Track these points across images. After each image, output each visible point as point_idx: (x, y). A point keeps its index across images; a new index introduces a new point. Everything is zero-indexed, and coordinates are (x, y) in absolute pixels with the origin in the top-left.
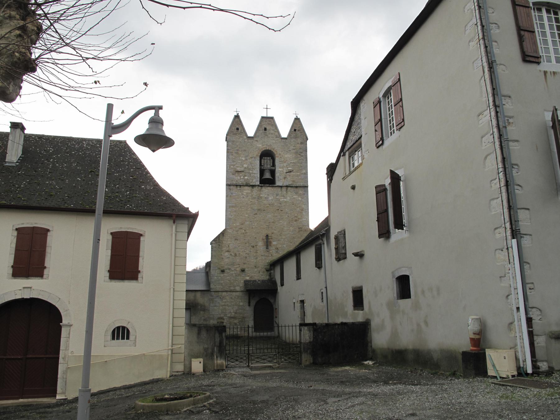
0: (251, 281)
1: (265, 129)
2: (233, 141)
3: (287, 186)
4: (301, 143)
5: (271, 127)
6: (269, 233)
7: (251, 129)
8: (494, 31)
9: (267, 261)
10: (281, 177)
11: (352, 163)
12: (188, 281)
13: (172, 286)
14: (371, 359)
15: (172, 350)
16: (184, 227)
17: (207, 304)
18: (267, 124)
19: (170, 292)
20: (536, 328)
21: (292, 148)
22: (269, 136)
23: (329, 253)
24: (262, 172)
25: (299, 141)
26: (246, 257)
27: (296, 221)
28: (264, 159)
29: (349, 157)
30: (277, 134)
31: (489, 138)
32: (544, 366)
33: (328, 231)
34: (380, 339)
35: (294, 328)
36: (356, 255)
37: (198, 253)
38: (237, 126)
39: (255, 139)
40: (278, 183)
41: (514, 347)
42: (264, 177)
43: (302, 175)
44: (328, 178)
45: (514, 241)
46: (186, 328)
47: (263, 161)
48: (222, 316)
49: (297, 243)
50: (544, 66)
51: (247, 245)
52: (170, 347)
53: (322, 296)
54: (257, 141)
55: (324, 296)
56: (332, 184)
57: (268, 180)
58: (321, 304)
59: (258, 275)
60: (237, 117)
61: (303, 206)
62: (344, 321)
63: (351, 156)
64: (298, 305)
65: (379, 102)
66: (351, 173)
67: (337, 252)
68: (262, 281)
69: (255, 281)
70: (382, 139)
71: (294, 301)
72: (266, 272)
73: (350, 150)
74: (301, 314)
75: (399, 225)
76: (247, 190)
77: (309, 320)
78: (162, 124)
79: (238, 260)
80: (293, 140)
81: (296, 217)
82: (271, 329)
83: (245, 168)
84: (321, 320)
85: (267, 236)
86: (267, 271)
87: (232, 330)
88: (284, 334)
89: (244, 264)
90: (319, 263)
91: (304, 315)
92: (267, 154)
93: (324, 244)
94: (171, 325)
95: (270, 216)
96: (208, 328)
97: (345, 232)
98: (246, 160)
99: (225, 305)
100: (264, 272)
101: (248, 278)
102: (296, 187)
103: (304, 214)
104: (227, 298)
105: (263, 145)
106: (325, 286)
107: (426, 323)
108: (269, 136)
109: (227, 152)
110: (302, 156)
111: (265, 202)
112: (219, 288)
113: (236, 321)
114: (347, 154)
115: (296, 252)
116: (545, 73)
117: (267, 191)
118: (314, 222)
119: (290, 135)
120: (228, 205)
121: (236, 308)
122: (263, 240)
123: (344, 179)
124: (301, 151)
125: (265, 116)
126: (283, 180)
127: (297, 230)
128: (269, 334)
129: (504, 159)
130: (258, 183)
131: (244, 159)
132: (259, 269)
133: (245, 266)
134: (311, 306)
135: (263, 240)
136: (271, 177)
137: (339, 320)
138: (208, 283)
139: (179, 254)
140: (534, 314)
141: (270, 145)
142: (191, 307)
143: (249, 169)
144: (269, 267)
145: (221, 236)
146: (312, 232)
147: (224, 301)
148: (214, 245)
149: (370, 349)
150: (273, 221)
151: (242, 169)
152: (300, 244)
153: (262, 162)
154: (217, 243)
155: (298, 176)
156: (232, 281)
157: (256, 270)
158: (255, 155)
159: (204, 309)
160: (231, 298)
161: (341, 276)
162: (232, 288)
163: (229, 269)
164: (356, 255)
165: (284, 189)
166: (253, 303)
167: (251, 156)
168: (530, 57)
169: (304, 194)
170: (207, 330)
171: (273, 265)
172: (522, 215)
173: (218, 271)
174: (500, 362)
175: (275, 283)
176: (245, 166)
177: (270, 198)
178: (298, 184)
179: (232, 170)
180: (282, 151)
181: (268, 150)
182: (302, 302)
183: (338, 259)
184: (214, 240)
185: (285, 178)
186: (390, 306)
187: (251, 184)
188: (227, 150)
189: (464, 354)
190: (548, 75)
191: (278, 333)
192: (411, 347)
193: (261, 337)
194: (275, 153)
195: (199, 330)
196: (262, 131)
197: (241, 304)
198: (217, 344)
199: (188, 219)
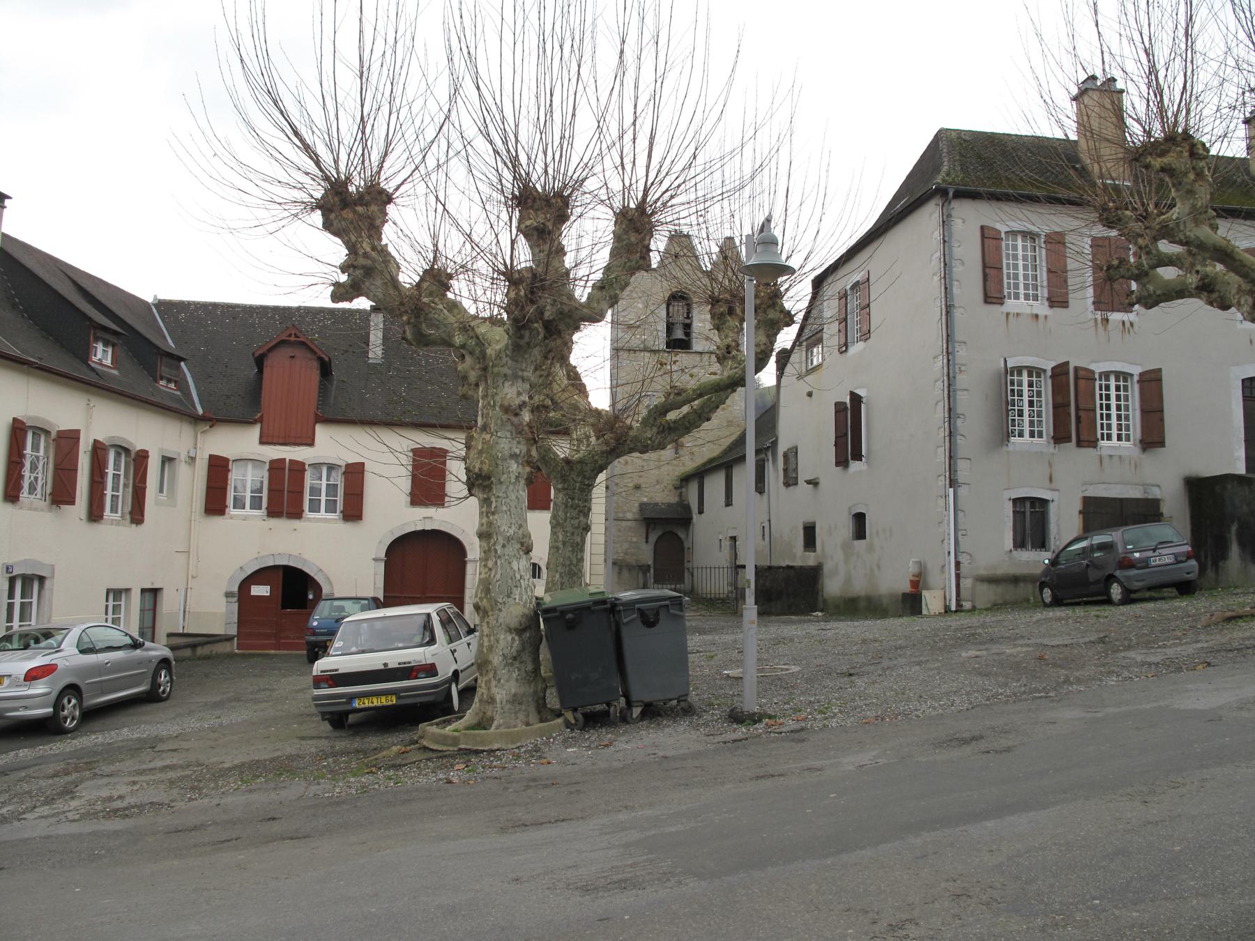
8: (957, 270)
14: (822, 611)
20: (963, 570)
24: (670, 328)
31: (939, 384)
32: (967, 605)
34: (832, 586)
36: (809, 482)
41: (944, 589)
45: (951, 490)
50: (1011, 305)
55: (766, 531)
58: (762, 543)
63: (809, 348)
64: (727, 544)
65: (846, 296)
67: (786, 475)
69: (657, 504)
70: (846, 345)
75: (858, 456)
101: (645, 500)
107: (879, 567)
116: (1008, 314)
121: (626, 545)
129: (950, 409)
130: (663, 346)
133: (641, 481)
137: (784, 564)
140: (964, 560)
149: (820, 598)
161: (789, 508)
162: (621, 515)
164: (809, 482)
166: (653, 538)
168: (992, 296)
171: (685, 480)
172: (962, 465)
174: (932, 601)
175: (687, 508)
182: (734, 539)
183: (787, 484)
186: (846, 547)
189: (904, 594)
190: (1011, 317)
192: (863, 594)
197: (634, 539)
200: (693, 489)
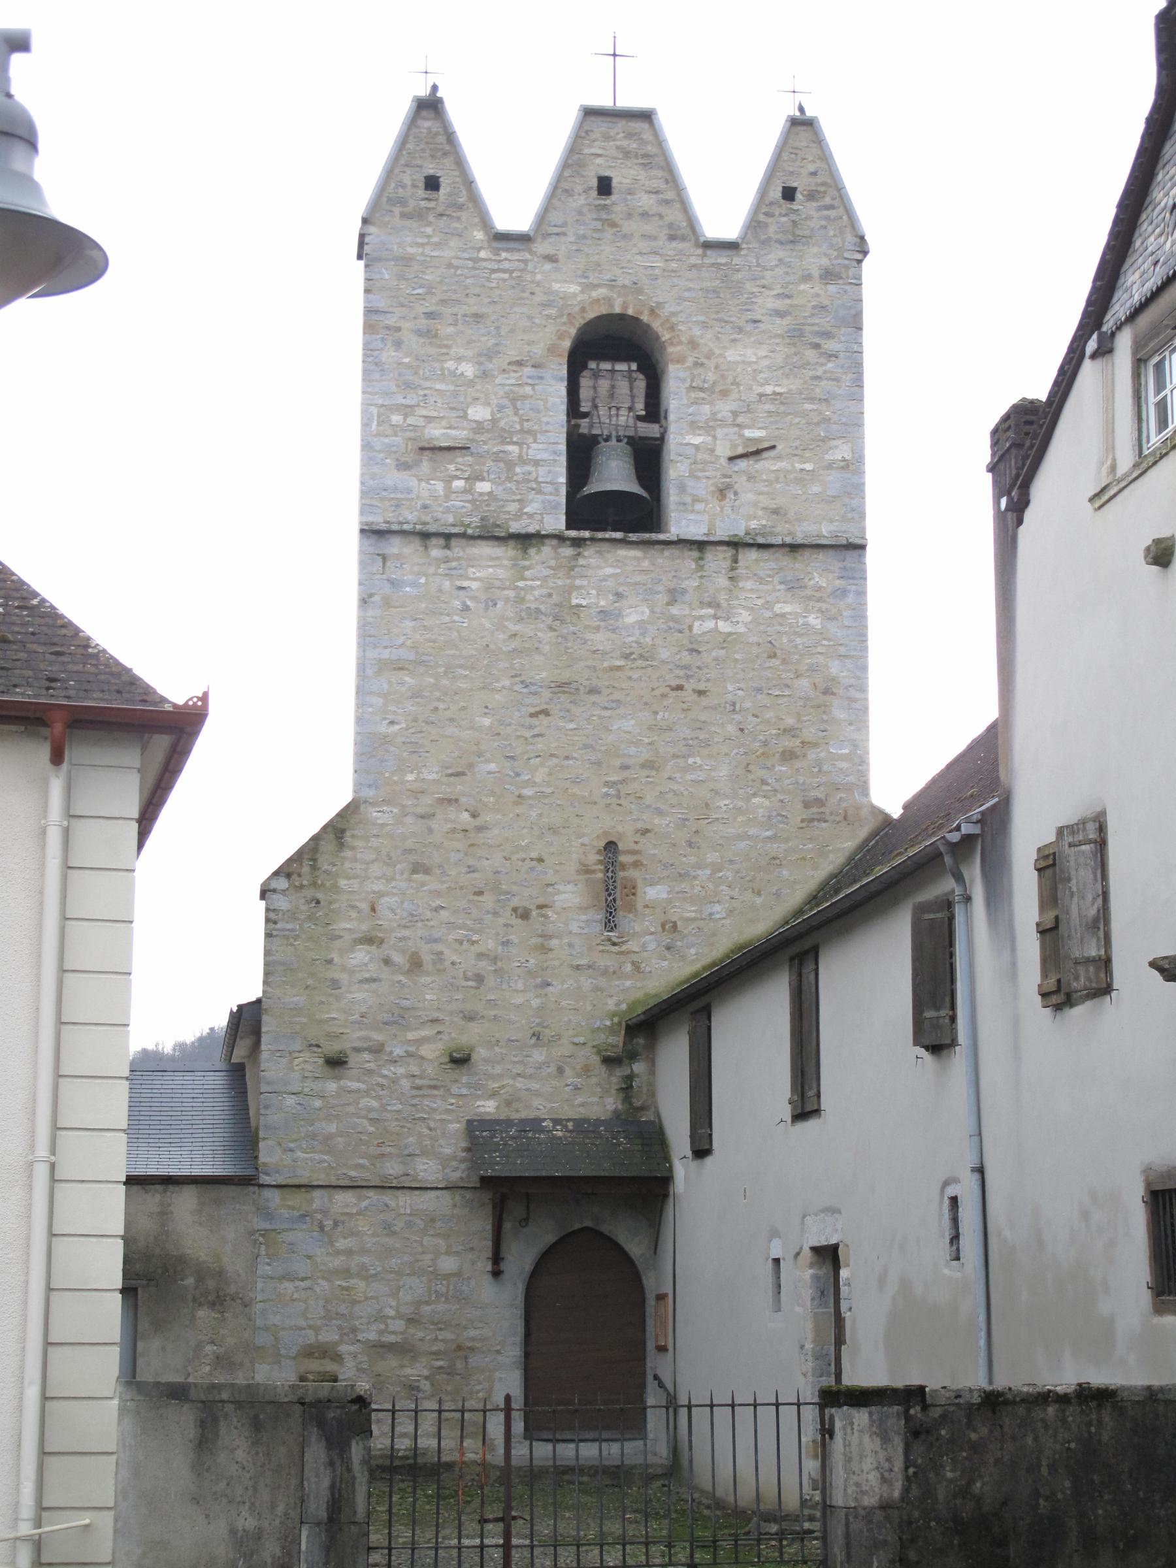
0: (509, 1122)
1: (605, 186)
2: (406, 260)
3: (735, 544)
4: (829, 276)
5: (642, 175)
6: (624, 830)
7: (513, 182)
9: (611, 1004)
10: (702, 488)
11: (1152, 399)
12: (142, 1123)
13: (42, 1151)
15: (38, 1545)
16: (116, 786)
17: (235, 1265)
18: (616, 154)
19: (30, 1188)
21: (772, 303)
22: (629, 226)
23: (999, 960)
24: (581, 453)
25: (815, 258)
26: (480, 979)
27: (789, 756)
28: (596, 375)
29: (1139, 363)
30: (674, 215)
33: (997, 822)
35: (788, 1413)
37: (189, 948)
38: (427, 164)
39: (542, 248)
40: (682, 522)
42: (593, 487)
43: (833, 476)
44: (998, 494)
46: (122, 1410)
47: (585, 382)
48: (329, 1336)
49: (796, 896)
51: (488, 900)
52: (26, 1529)
53: (955, 1221)
54: (551, 259)
55: (967, 1219)
56: (1025, 533)
57: (617, 502)
58: (949, 1271)
59: (553, 1089)
60: (429, 107)
61: (835, 668)
62: (1098, 1378)
64: (801, 1277)
66: (1145, 463)
68: (579, 1123)
69: (535, 1124)
71: (776, 1251)
72: (601, 1070)
73: (1144, 320)
74: (817, 1330)
76: (488, 564)
77: (867, 1368)
78: (31, 144)
79: (429, 994)
80: (775, 254)
81: (789, 732)
82: (630, 1421)
83: (479, 428)
84: (953, 1370)
85: (611, 847)
86: (609, 1061)
87: (428, 1423)
88: (701, 1457)
89: (470, 1018)
90: (936, 1021)
91: (840, 1341)
92: (615, 345)
93: (968, 899)
94: (32, 1393)
95: (629, 724)
96: (259, 1411)
97: (1102, 829)
98: (485, 375)
99: (346, 1273)
100: (587, 1069)
101: (488, 1107)
102: (794, 548)
103: (839, 714)
104: (363, 1225)
105: (587, 287)
106: (971, 1160)
108: (629, 226)
109: (369, 328)
110: (832, 356)
111: (600, 639)
112: (307, 1163)
113: (416, 1371)
114: (1124, 343)
115: (794, 950)
117: (612, 566)
118: (898, 771)
119: (754, 224)
120: (372, 654)
121: (415, 1288)
122: (586, 870)
123: (1101, 498)
124: (825, 322)
125: (606, 102)
126: (714, 505)
127: (797, 814)
128: (613, 1451)
130: (557, 522)
131: (468, 369)
132: (565, 1049)
133: (470, 1035)
134: (882, 1282)
135: (586, 870)
136: (634, 487)
137: (1065, 1376)
138: (245, 1135)
139: (79, 953)
141: (636, 288)
142: (150, 1280)
143: (505, 436)
144: (618, 1040)
145: (327, 847)
146: (887, 832)
147: (341, 1244)
148: (282, 903)
150: (645, 755)
151: (459, 435)
152: (814, 899)
153: (585, 393)
154: (303, 884)
155: (803, 479)
156: (393, 1126)
157: (539, 1056)
158: (538, 350)
159: (219, 1295)
160: (388, 1229)
162: (392, 1168)
163: (377, 1050)
165: (718, 560)
166: (521, 1257)
167: (513, 354)
169: (844, 592)
170: (257, 1425)
171: (645, 1027)
173: (312, 1062)
175: (653, 1139)
176: (479, 413)
177: (631, 618)
178: (802, 532)
179: (403, 444)
180: (705, 326)
181: (622, 317)
182: (829, 1255)
183: (1059, 997)
184: (285, 871)
185: (722, 492)
187: (515, 527)
188: (369, 311)
191: (675, 1451)
193: (563, 1473)
194: (665, 336)
195: (202, 1424)
196: (583, 198)
197: (448, 1264)
198: (318, 1508)
199: (160, 735)
200: (674, 1054)
